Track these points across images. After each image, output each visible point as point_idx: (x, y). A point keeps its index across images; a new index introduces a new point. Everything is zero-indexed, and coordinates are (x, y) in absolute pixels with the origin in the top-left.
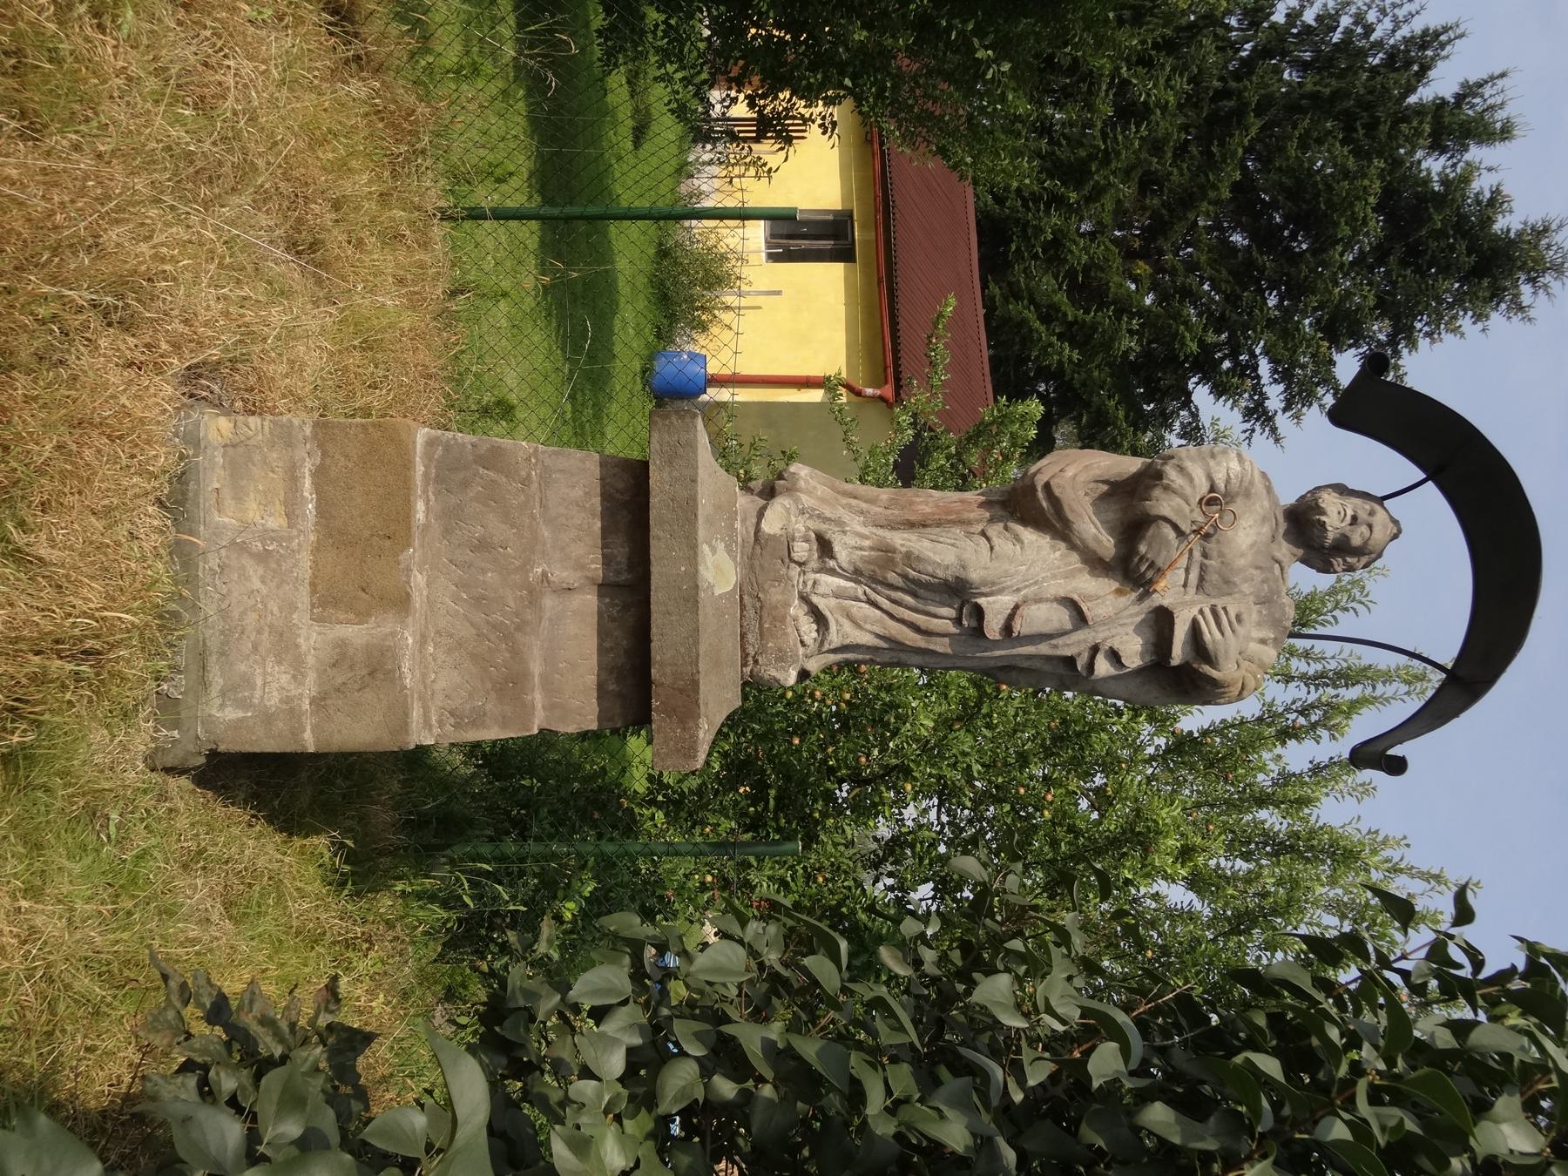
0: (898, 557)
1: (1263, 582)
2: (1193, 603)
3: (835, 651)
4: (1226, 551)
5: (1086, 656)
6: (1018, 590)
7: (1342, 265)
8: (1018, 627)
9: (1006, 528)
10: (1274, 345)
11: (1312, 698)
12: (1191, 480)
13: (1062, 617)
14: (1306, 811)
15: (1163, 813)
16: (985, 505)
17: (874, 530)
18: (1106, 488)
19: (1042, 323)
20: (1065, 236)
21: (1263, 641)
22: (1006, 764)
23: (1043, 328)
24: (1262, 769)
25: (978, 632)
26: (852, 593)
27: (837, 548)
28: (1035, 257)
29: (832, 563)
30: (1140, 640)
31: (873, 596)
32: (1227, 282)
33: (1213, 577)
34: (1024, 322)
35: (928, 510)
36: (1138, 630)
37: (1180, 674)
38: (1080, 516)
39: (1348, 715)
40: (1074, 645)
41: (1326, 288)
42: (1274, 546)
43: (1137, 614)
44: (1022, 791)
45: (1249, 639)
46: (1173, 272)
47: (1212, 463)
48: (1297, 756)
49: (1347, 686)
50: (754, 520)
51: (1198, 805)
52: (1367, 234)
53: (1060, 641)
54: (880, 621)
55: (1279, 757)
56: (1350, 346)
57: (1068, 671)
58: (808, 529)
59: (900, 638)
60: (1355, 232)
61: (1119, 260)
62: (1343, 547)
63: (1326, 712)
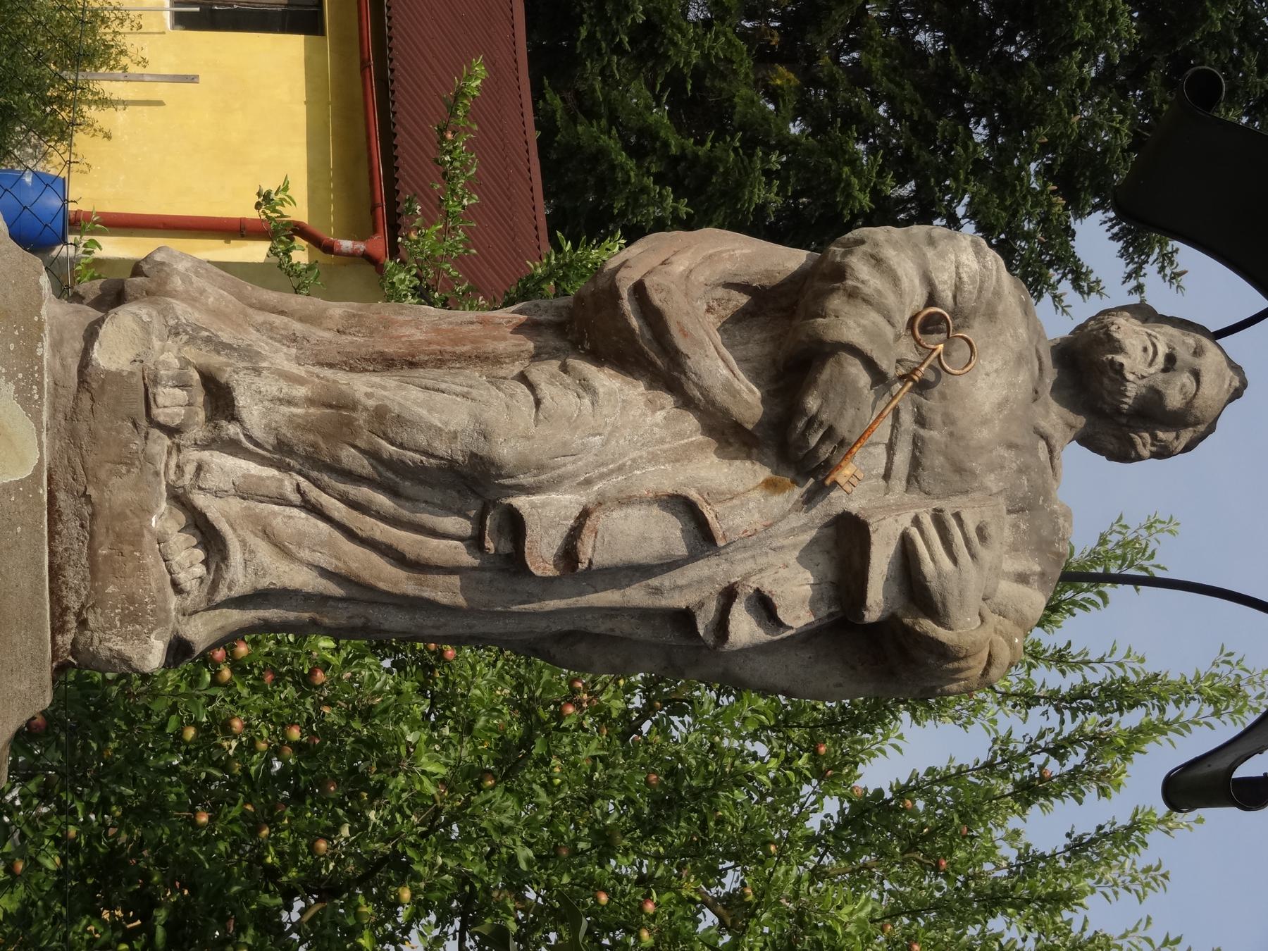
0: (361, 418)
1: (1020, 471)
2: (900, 507)
3: (240, 602)
4: (958, 413)
5: (712, 606)
6: (588, 482)
7: (1082, 81)
8: (590, 551)
9: (564, 368)
10: (985, 202)
11: (1069, 728)
12: (895, 281)
13: (668, 534)
14: (1066, 915)
15: (843, 915)
16: (529, 328)
17: (317, 370)
18: (743, 300)
19: (630, 156)
20: (664, 20)
21: (1022, 578)
22: (575, 853)
23: (631, 164)
24: (990, 853)
25: (513, 562)
26: (273, 490)
27: (242, 400)
28: (618, 49)
29: (232, 430)
30: (808, 576)
31: (314, 494)
32: (913, 102)
33: (935, 461)
34: (601, 154)
35: (419, 336)
36: (805, 557)
37: (884, 647)
38: (699, 344)
39: (1126, 753)
40: (690, 588)
41: (1060, 114)
42: (1038, 409)
43: (804, 528)
44: (603, 898)
45: (998, 573)
46: (831, 85)
47: (930, 253)
48: (1047, 828)
49: (1120, 710)
50: (79, 345)
51: (893, 914)
52: (1117, 38)
53: (665, 580)
54: (330, 544)
55: (1017, 833)
56: (1095, 208)
57: (681, 647)
58: (186, 363)
59: (366, 576)
60: (1100, 32)
61: (748, 63)
62: (1152, 412)
63: (1091, 750)
